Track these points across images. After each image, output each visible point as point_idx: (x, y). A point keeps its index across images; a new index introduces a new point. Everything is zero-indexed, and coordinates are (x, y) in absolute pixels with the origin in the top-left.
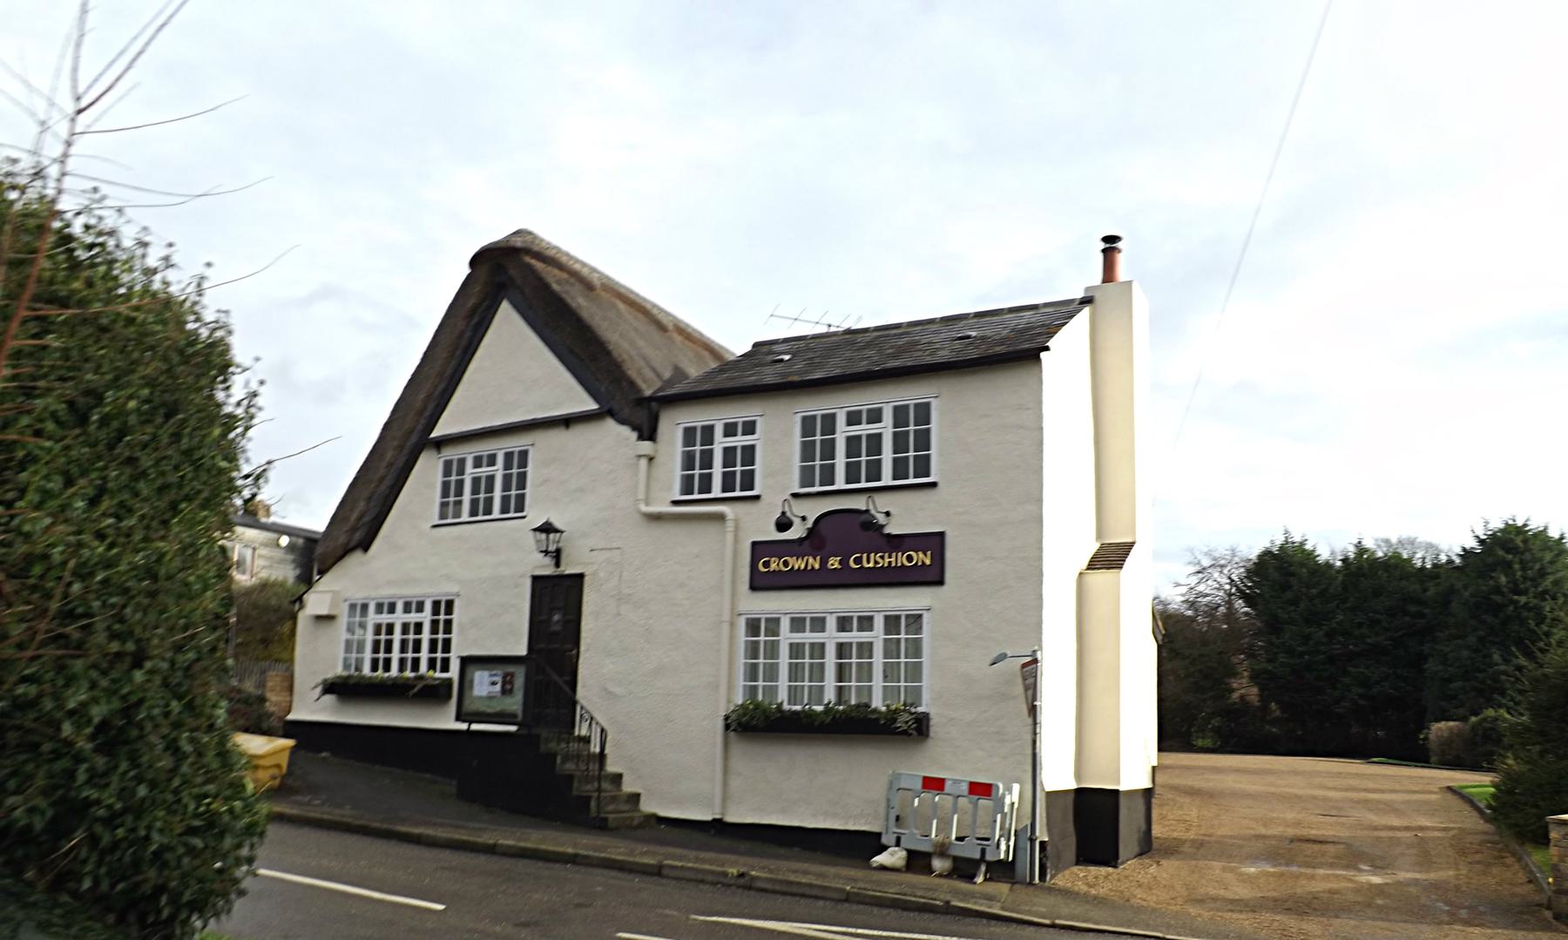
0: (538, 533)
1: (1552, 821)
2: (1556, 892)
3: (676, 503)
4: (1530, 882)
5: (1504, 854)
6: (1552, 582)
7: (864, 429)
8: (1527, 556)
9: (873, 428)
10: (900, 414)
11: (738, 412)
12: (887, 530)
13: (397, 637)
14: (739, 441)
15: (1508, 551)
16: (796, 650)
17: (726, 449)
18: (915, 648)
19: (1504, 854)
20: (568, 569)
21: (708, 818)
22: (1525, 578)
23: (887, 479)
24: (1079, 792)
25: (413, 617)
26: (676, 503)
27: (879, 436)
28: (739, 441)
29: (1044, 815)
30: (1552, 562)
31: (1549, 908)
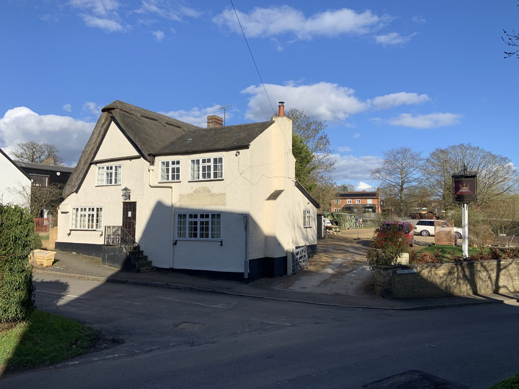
0: (123, 191)
3: (159, 183)
7: (206, 164)
9: (209, 164)
10: (215, 160)
11: (175, 158)
12: (212, 192)
13: (199, 226)
14: (176, 166)
16: (202, 223)
17: (172, 168)
18: (219, 223)
20: (132, 200)
21: (169, 267)
23: (212, 177)
25: (91, 213)
26: (159, 183)
27: (210, 166)
28: (176, 166)
29: (477, 298)
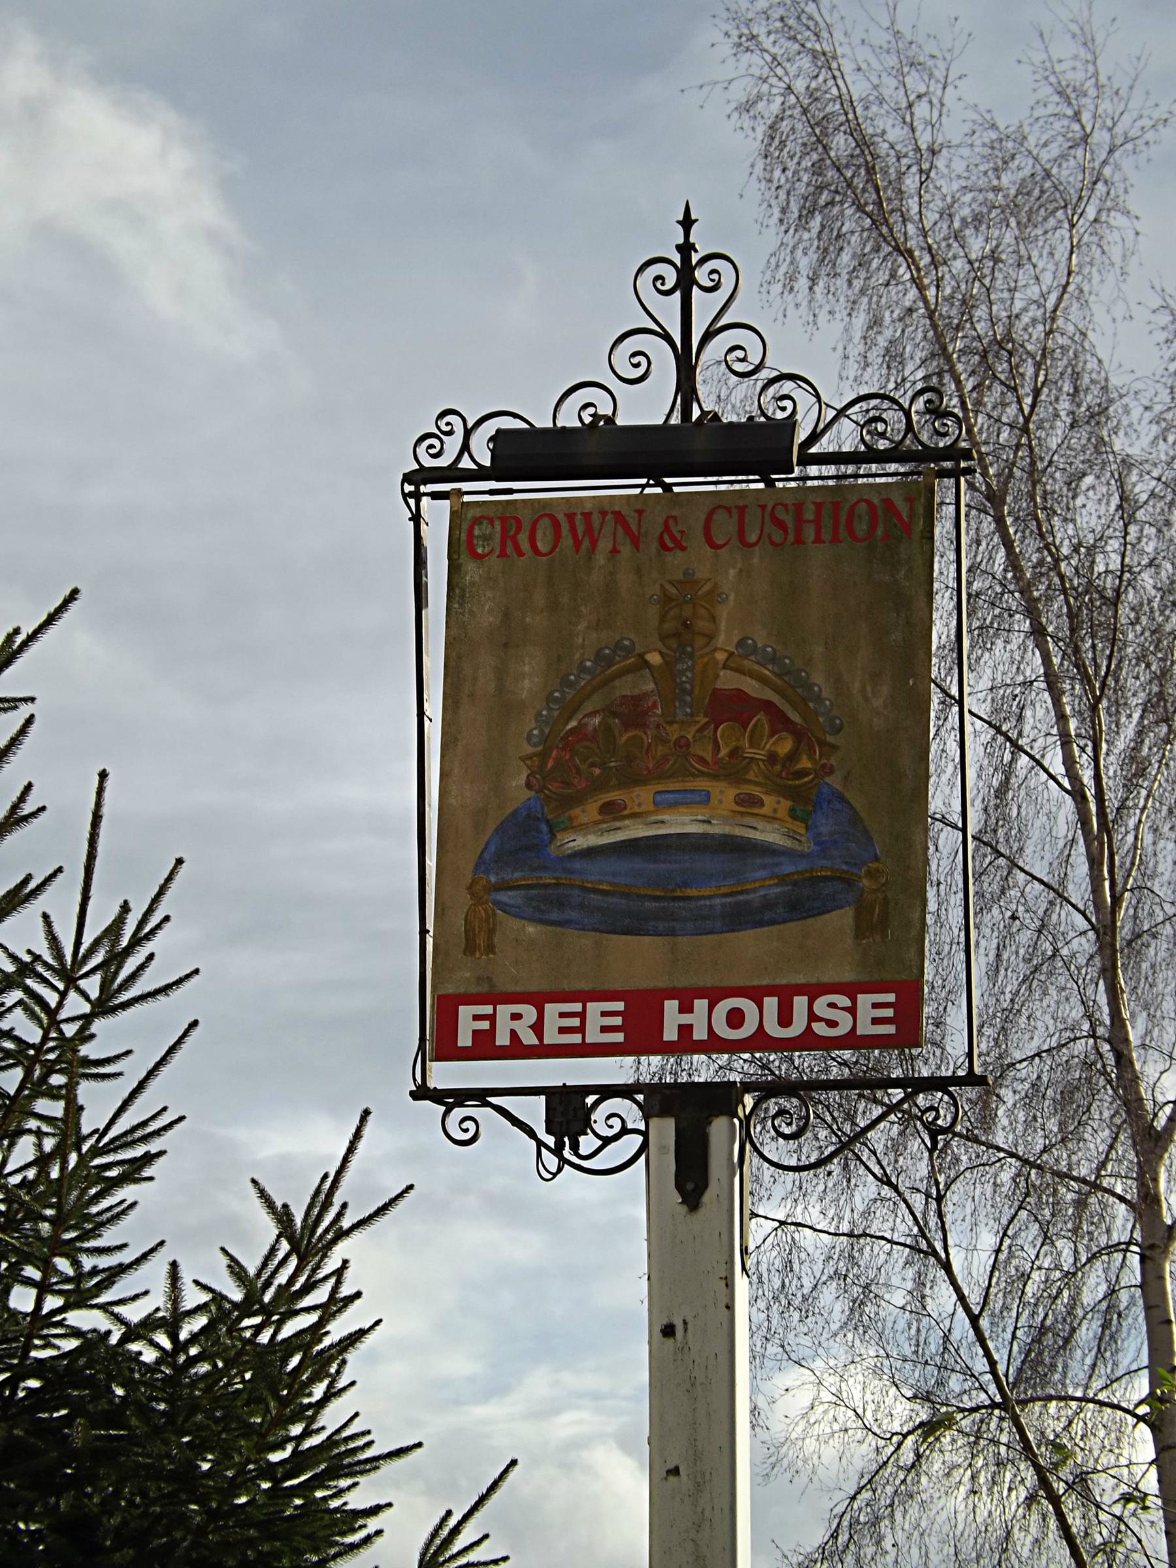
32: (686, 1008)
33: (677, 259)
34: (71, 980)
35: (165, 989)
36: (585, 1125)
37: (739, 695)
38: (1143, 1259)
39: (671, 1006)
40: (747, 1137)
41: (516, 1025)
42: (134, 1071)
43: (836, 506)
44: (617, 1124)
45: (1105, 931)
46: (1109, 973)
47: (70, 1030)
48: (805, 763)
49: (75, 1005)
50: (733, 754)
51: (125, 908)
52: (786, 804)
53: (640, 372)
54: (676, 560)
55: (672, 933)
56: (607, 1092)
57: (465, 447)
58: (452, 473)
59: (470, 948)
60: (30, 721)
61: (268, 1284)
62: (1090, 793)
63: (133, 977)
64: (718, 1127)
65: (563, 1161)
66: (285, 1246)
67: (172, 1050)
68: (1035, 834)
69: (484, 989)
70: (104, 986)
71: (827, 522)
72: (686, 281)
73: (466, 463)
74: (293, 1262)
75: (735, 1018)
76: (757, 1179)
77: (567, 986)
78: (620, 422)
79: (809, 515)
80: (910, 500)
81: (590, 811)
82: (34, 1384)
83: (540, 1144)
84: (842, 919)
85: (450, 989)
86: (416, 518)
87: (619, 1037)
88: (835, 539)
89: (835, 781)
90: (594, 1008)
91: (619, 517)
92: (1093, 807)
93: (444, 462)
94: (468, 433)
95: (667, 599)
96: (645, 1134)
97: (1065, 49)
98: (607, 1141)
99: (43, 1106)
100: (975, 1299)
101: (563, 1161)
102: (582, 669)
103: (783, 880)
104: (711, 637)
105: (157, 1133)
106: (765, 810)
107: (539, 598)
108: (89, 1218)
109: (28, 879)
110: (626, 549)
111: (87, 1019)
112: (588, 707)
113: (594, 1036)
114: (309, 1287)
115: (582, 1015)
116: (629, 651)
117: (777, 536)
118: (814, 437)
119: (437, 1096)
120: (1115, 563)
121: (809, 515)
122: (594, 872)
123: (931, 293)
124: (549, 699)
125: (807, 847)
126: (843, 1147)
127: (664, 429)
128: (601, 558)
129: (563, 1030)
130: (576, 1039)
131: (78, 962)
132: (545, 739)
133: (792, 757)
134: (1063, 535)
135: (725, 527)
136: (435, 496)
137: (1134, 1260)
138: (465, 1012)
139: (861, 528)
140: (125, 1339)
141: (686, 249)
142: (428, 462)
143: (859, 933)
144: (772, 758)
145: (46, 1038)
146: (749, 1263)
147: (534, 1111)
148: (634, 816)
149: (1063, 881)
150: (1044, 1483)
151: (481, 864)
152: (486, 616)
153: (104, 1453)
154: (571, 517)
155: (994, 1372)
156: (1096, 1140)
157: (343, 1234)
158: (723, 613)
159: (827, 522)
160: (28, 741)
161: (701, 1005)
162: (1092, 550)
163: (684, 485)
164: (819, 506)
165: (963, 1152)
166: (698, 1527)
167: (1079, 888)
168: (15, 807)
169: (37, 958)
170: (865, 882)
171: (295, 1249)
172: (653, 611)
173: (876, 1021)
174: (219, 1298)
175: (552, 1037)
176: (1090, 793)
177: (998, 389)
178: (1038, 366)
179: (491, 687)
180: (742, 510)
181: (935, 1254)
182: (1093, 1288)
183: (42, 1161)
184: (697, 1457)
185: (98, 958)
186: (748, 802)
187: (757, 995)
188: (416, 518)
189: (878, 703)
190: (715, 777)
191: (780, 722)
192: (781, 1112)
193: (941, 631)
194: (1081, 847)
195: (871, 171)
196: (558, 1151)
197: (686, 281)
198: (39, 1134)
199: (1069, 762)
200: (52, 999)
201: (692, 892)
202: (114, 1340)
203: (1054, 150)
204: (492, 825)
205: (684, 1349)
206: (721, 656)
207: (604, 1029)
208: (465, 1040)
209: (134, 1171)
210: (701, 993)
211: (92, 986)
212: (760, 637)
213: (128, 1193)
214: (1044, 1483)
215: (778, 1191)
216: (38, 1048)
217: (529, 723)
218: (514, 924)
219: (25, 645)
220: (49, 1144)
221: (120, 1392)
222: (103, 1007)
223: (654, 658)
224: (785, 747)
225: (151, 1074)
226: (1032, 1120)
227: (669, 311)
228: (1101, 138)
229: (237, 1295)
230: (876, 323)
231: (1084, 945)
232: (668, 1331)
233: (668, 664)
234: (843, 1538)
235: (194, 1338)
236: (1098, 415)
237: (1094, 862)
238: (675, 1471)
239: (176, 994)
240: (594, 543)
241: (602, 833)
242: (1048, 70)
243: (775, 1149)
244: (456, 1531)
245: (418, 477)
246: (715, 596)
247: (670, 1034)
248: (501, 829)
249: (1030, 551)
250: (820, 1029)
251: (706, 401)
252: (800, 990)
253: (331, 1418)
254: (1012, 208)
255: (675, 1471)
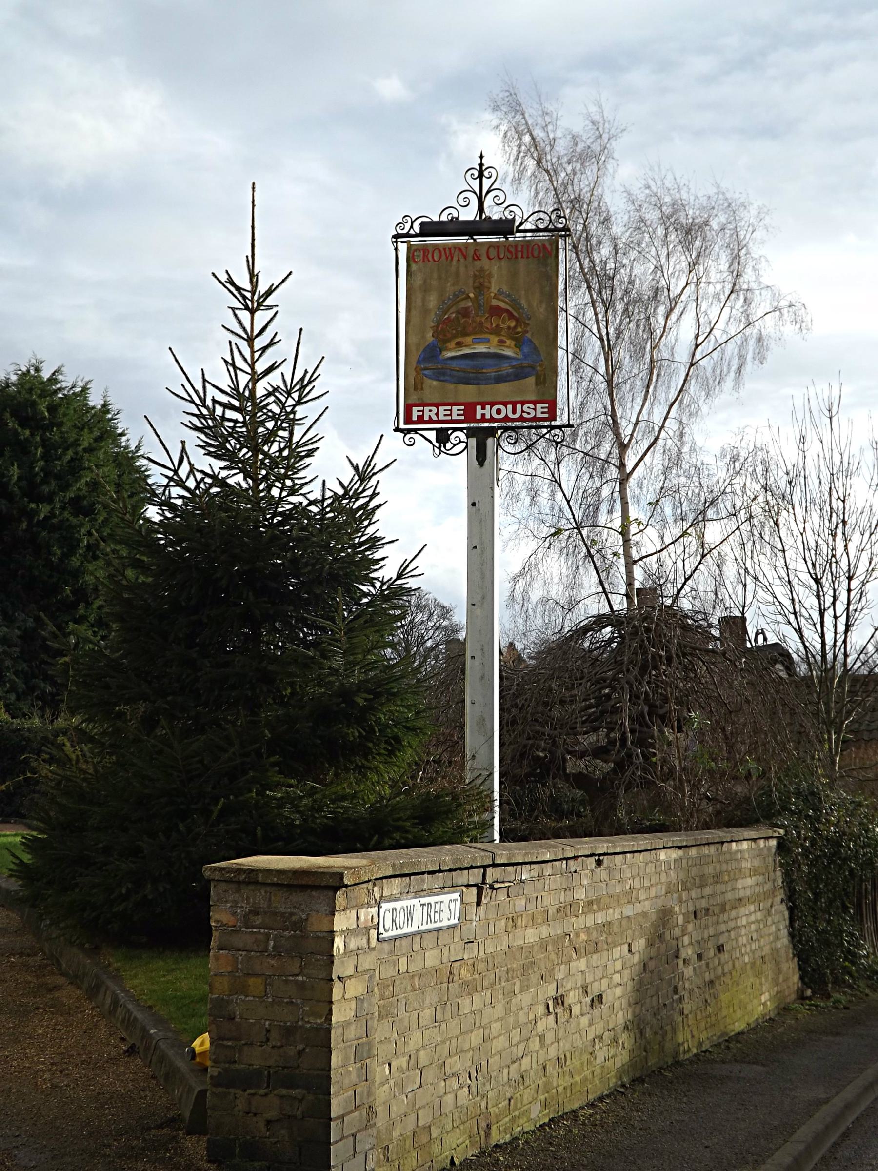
1: (217, 876)
2: (217, 1082)
4: (131, 1051)
5: (49, 980)
6: (87, 484)
8: (54, 435)
15: (24, 422)
19: (49, 980)
22: (48, 473)
24: (332, 932)
30: (90, 450)
31: (197, 1127)
32: (483, 408)
33: (478, 168)
34: (289, 394)
35: (318, 397)
36: (448, 440)
37: (498, 307)
38: (620, 483)
39: (479, 408)
40: (499, 444)
41: (430, 414)
42: (308, 422)
43: (528, 246)
44: (458, 439)
45: (609, 382)
46: (611, 395)
47: (289, 409)
48: (519, 329)
49: (291, 402)
50: (497, 326)
51: (306, 372)
52: (513, 343)
53: (466, 204)
54: (478, 263)
55: (478, 384)
56: (455, 430)
57: (412, 227)
58: (408, 235)
59: (416, 389)
60: (277, 313)
61: (351, 489)
62: (605, 338)
63: (308, 393)
64: (490, 442)
65: (441, 451)
66: (356, 478)
67: (320, 416)
68: (588, 352)
69: (420, 402)
70: (300, 396)
71: (525, 251)
72: (481, 175)
73: (412, 232)
74: (359, 482)
75: (499, 412)
76: (502, 458)
77: (446, 401)
78: (461, 218)
79: (519, 249)
80: (551, 245)
81: (452, 345)
82: (280, 518)
83: (434, 446)
84: (531, 380)
85: (410, 402)
86: (396, 249)
87: (462, 418)
88: (528, 257)
89: (528, 335)
90: (455, 408)
91: (460, 250)
92: (606, 343)
93: (405, 231)
94: (412, 222)
95: (475, 276)
96: (467, 443)
97: (593, 109)
98: (455, 445)
99: (281, 433)
100: (568, 495)
101: (441, 451)
102: (449, 299)
103: (513, 367)
104: (489, 288)
105: (316, 442)
106: (507, 344)
107: (435, 275)
108: (295, 468)
109: (276, 362)
110: (462, 260)
111: (294, 406)
112: (451, 311)
113: (455, 417)
114: (364, 491)
115: (451, 410)
116: (464, 293)
117: (509, 256)
118: (521, 224)
119: (402, 431)
120: (613, 266)
121: (519, 249)
122: (454, 364)
123: (555, 183)
124: (439, 309)
125: (520, 356)
126: (528, 448)
127: (474, 221)
128: (454, 262)
129: (445, 415)
130: (449, 418)
131: (292, 388)
132: (438, 321)
133: (515, 327)
134: (596, 257)
135: (493, 253)
136: (402, 242)
137: (618, 483)
138: (415, 409)
139: (536, 253)
140: (309, 505)
141: (481, 165)
142: (400, 232)
143: (537, 384)
144: (509, 328)
145: (281, 412)
146: (499, 484)
147: (432, 435)
148: (466, 346)
149: (596, 365)
150: (588, 551)
151: (419, 362)
152: (418, 281)
153: (299, 540)
154: (445, 249)
155: (574, 518)
156: (606, 446)
157: (374, 474)
158: (493, 280)
159: (525, 251)
160: (276, 319)
161: (488, 407)
162: (606, 263)
163: (481, 239)
164: (522, 246)
165: (565, 451)
166: (482, 565)
167: (602, 369)
168: (272, 340)
169: (279, 387)
170: (539, 368)
171: (360, 478)
172: (471, 281)
173: (542, 413)
174: (335, 494)
175: (442, 417)
176: (605, 338)
177: (577, 213)
178: (588, 205)
179: (421, 304)
180: (498, 247)
181: (556, 481)
182: (606, 492)
183: (281, 451)
184: (482, 544)
185: (298, 387)
186: (501, 342)
187: (505, 404)
188: (396, 249)
189: (542, 310)
190: (491, 334)
191: (511, 316)
192: (509, 436)
193: (561, 287)
194: (602, 356)
195: (536, 147)
196: (439, 448)
197: (481, 175)
198: (280, 442)
199: (599, 329)
200: (283, 399)
201: (484, 371)
202: (304, 504)
203: (591, 140)
204: (422, 349)
205: (479, 510)
206: (492, 295)
207: (458, 415)
208: (415, 418)
209: (310, 453)
210: (488, 403)
211: (296, 396)
212: (505, 289)
213: (307, 461)
214: (588, 551)
215: (508, 462)
216: (279, 415)
217: (433, 316)
218: (430, 381)
219: (275, 289)
220: (282, 445)
221: (306, 521)
222: (299, 403)
223: (472, 295)
224: (513, 324)
225: (314, 423)
226: (586, 441)
227: (476, 185)
228: (605, 136)
229: (341, 492)
230: (537, 193)
231: (604, 386)
232: (474, 504)
233: (476, 297)
234: (527, 569)
235: (328, 506)
236: (607, 219)
237: (607, 361)
238: (475, 547)
239: (322, 399)
240: (452, 258)
241: (456, 351)
242: (588, 115)
243: (510, 449)
244: (408, 566)
245: (397, 236)
246: (490, 275)
247: (478, 417)
248: (424, 350)
249: (586, 263)
250: (525, 415)
251: (487, 212)
252: (519, 402)
253: (370, 530)
254: (580, 156)
255: (475, 547)
